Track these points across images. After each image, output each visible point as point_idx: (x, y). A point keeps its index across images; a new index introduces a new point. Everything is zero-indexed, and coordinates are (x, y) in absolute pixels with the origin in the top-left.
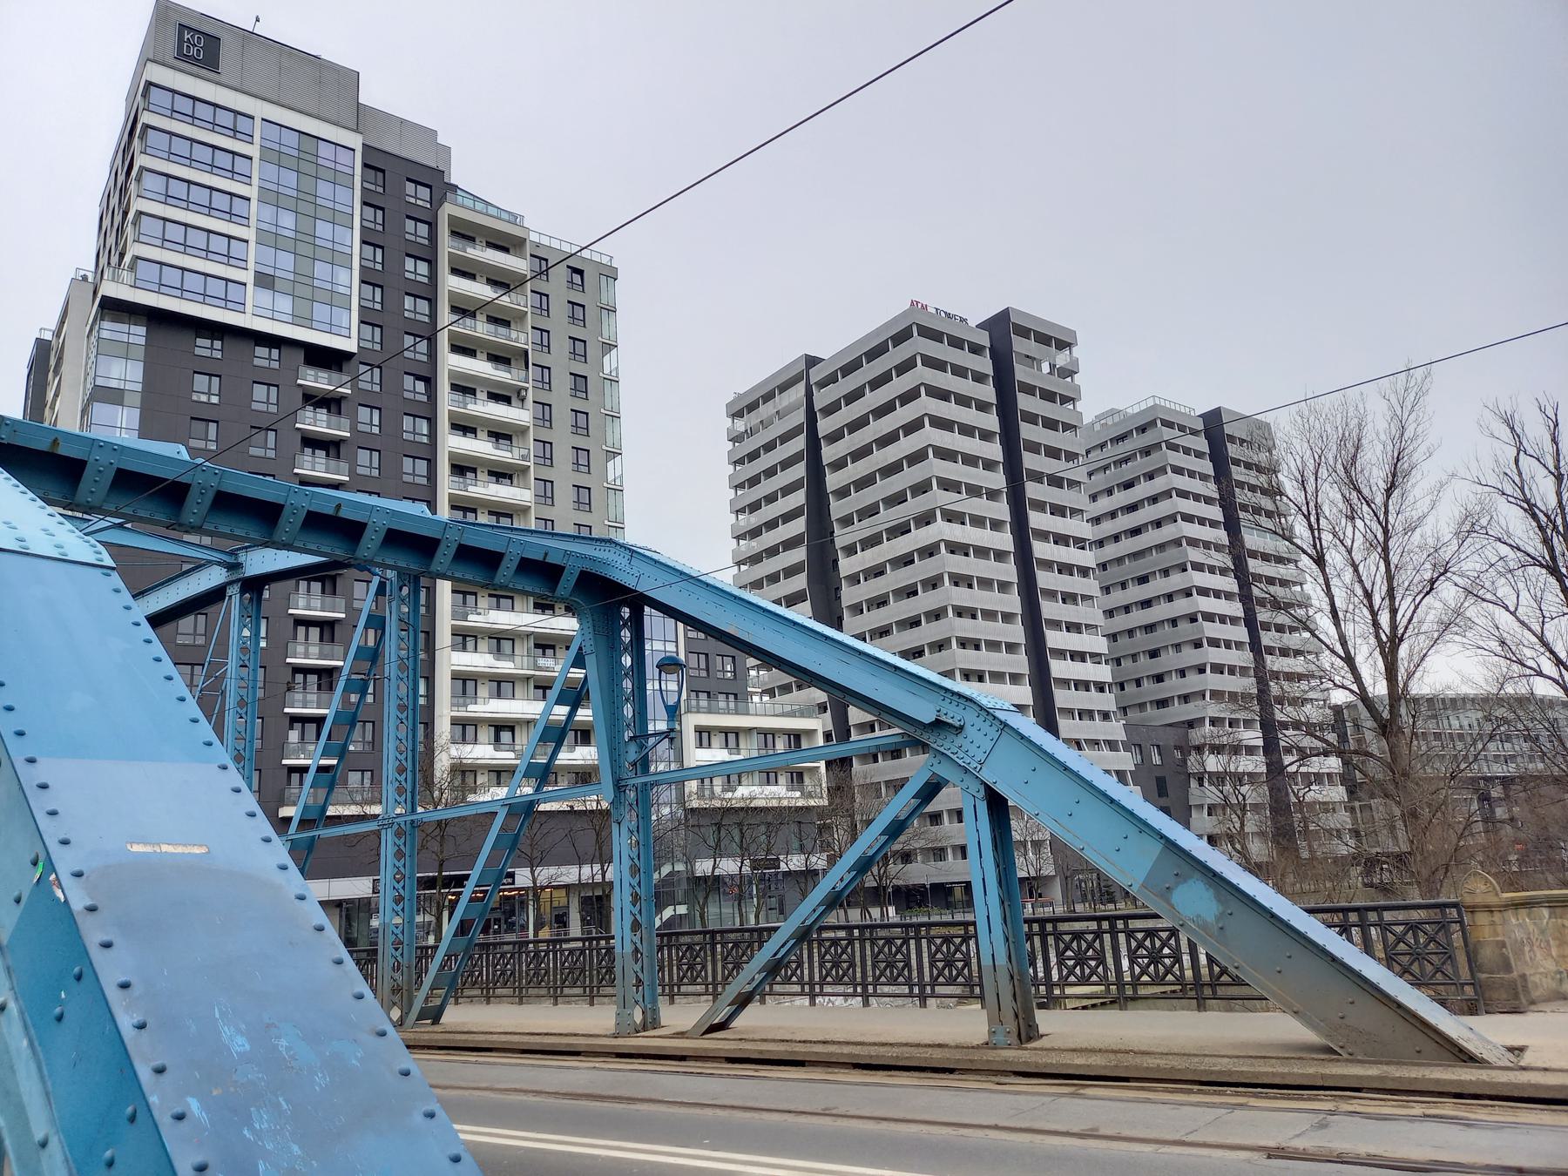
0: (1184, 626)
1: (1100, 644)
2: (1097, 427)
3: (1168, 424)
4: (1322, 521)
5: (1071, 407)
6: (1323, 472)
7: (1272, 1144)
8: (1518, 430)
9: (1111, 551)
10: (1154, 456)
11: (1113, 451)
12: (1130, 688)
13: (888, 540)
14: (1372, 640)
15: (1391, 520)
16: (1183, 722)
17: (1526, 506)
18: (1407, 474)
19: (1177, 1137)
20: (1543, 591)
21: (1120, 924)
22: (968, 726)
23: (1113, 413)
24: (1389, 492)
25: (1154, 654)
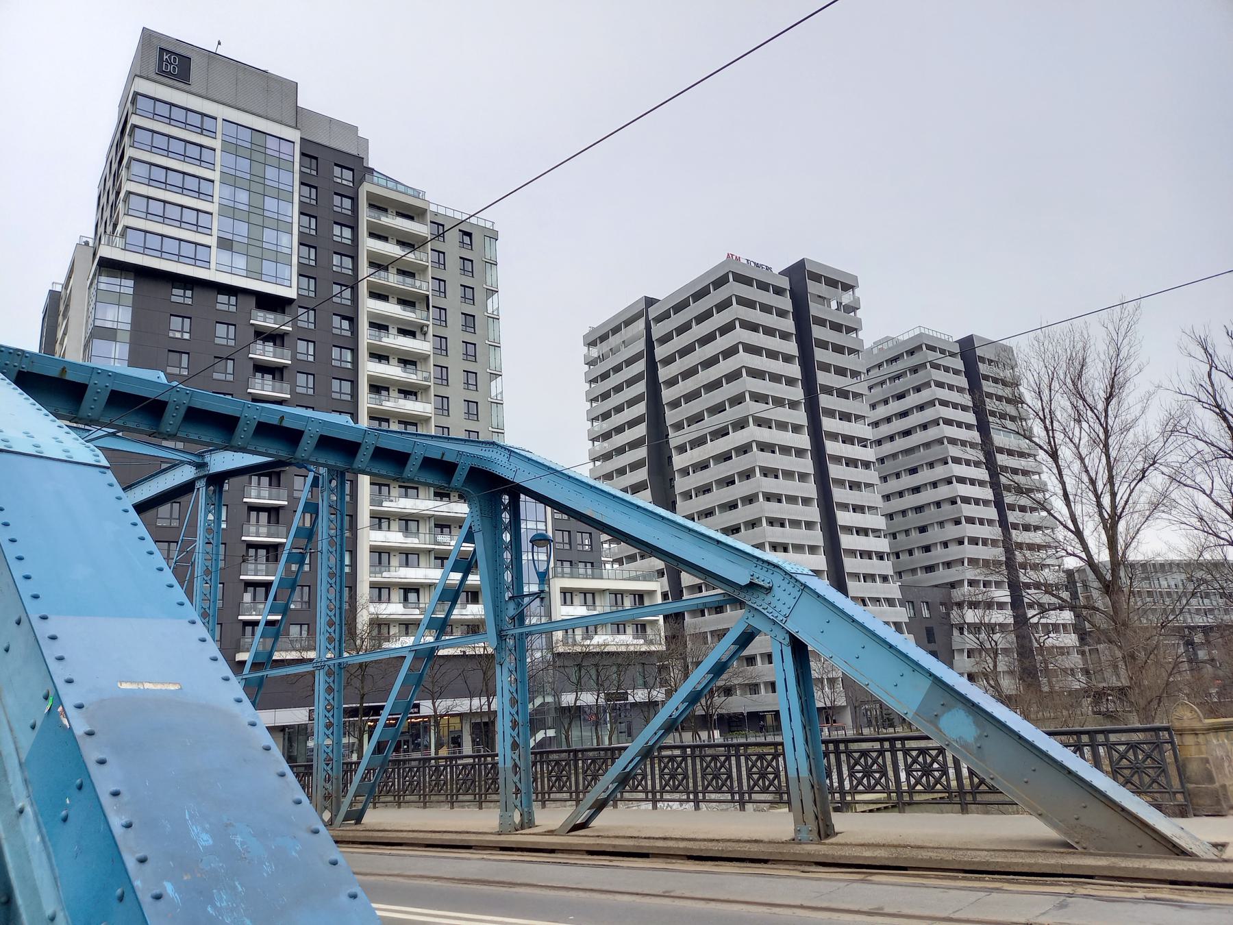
0: (946, 507)
1: (879, 522)
2: (875, 351)
3: (932, 348)
4: (1056, 424)
6: (1055, 385)
8: (1211, 351)
9: (888, 448)
10: (921, 373)
11: (888, 370)
13: (711, 440)
14: (1097, 518)
15: (1110, 422)
16: (947, 584)
17: (1218, 411)
22: (775, 588)
23: (887, 339)
24: (1108, 400)
25: (923, 529)
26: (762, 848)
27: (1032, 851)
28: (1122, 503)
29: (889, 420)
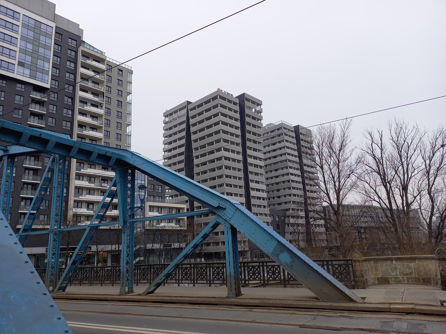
0: (286, 183)
1: (264, 187)
2: (267, 128)
4: (323, 157)
5: (260, 122)
7: (301, 324)
8: (373, 137)
9: (268, 162)
10: (281, 137)
13: (208, 155)
14: (334, 189)
15: (340, 158)
16: (285, 209)
18: (345, 146)
20: (376, 179)
21: (265, 264)
22: (227, 208)
23: (271, 124)
24: (340, 150)
25: (278, 190)
26: (216, 300)
27: (306, 300)
28: (342, 185)
29: (269, 152)
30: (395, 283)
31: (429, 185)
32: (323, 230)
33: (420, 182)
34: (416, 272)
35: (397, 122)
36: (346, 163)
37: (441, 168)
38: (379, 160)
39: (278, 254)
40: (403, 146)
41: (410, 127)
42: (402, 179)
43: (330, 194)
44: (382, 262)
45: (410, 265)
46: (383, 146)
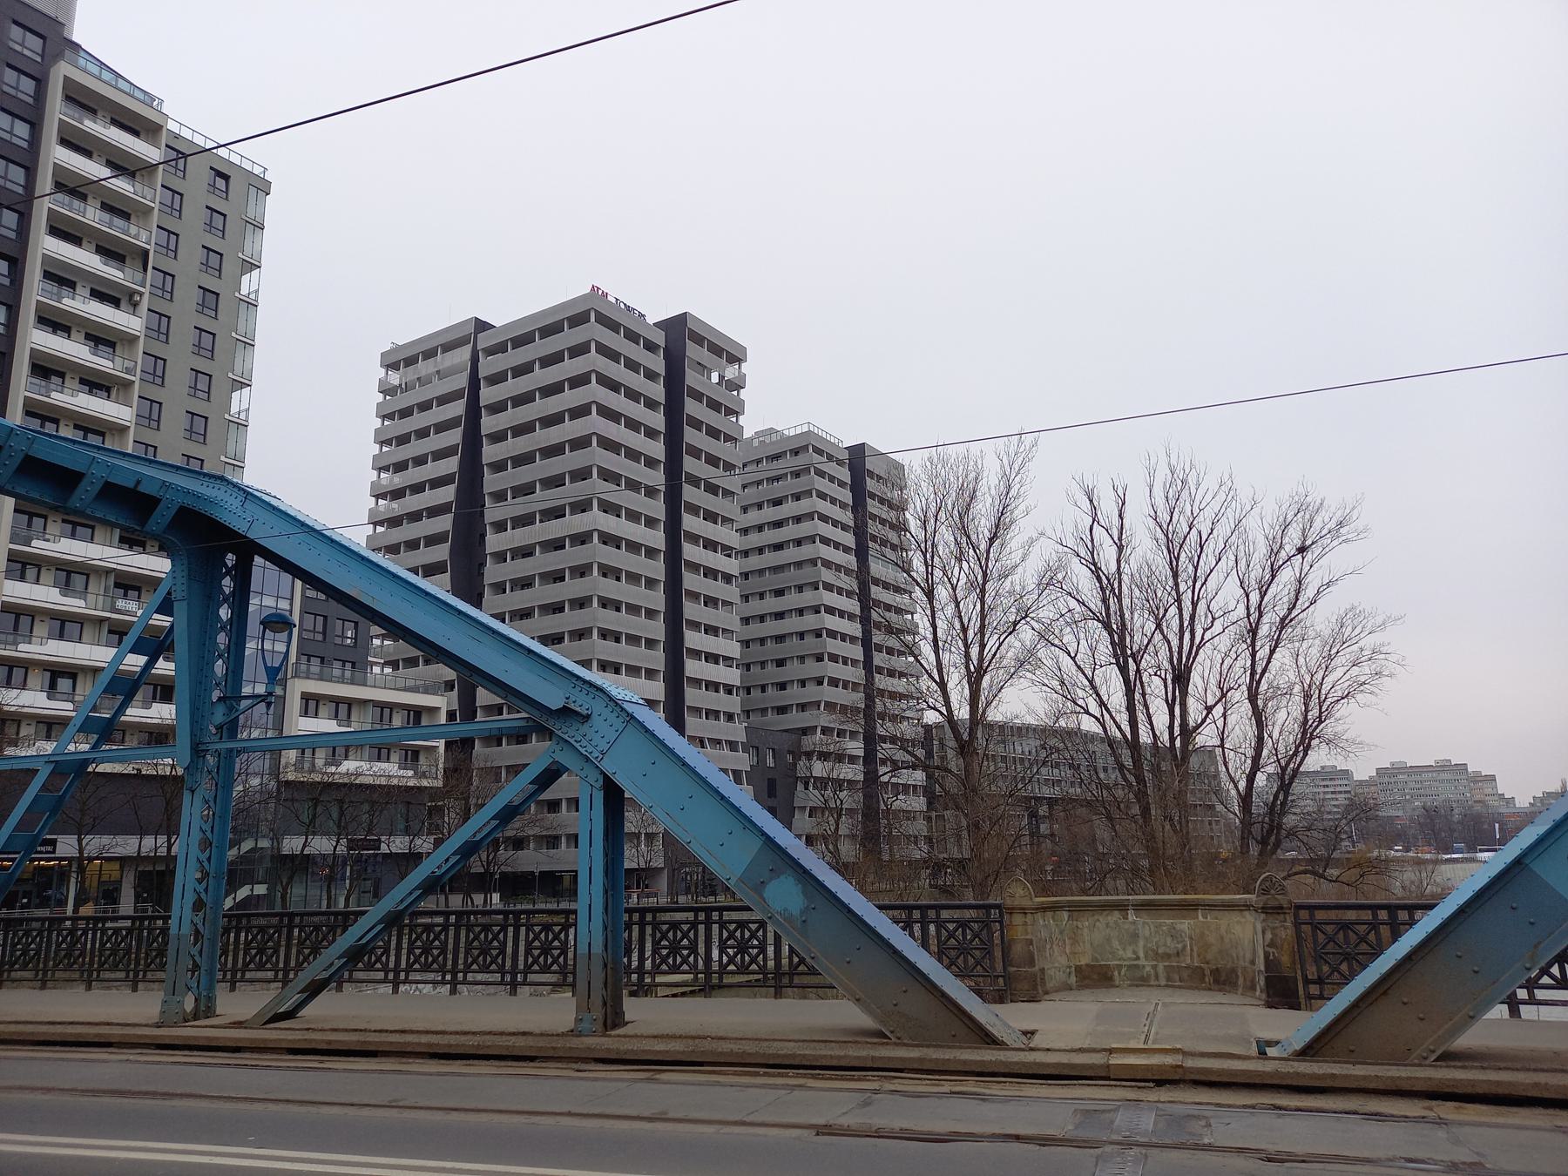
0: (810, 640)
1: (732, 648)
2: (756, 443)
3: (819, 451)
4: (936, 558)
5: (734, 420)
6: (942, 515)
7: (822, 1121)
8: (1096, 503)
9: (755, 562)
10: (803, 478)
12: (755, 693)
13: (541, 521)
14: (963, 670)
19: (737, 1118)
20: (1097, 642)
22: (595, 716)
23: (771, 431)
24: (991, 541)
25: (780, 663)
26: (530, 1041)
29: (760, 528)
30: (1130, 986)
31: (1252, 675)
32: (918, 803)
33: (1228, 661)
34: (1195, 949)
35: (1173, 462)
36: (1007, 583)
37: (1291, 620)
38: (1109, 580)
39: (762, 883)
40: (1183, 542)
41: (1210, 483)
42: (1175, 649)
43: (950, 685)
44: (1093, 915)
45: (1178, 927)
46: (1124, 536)
